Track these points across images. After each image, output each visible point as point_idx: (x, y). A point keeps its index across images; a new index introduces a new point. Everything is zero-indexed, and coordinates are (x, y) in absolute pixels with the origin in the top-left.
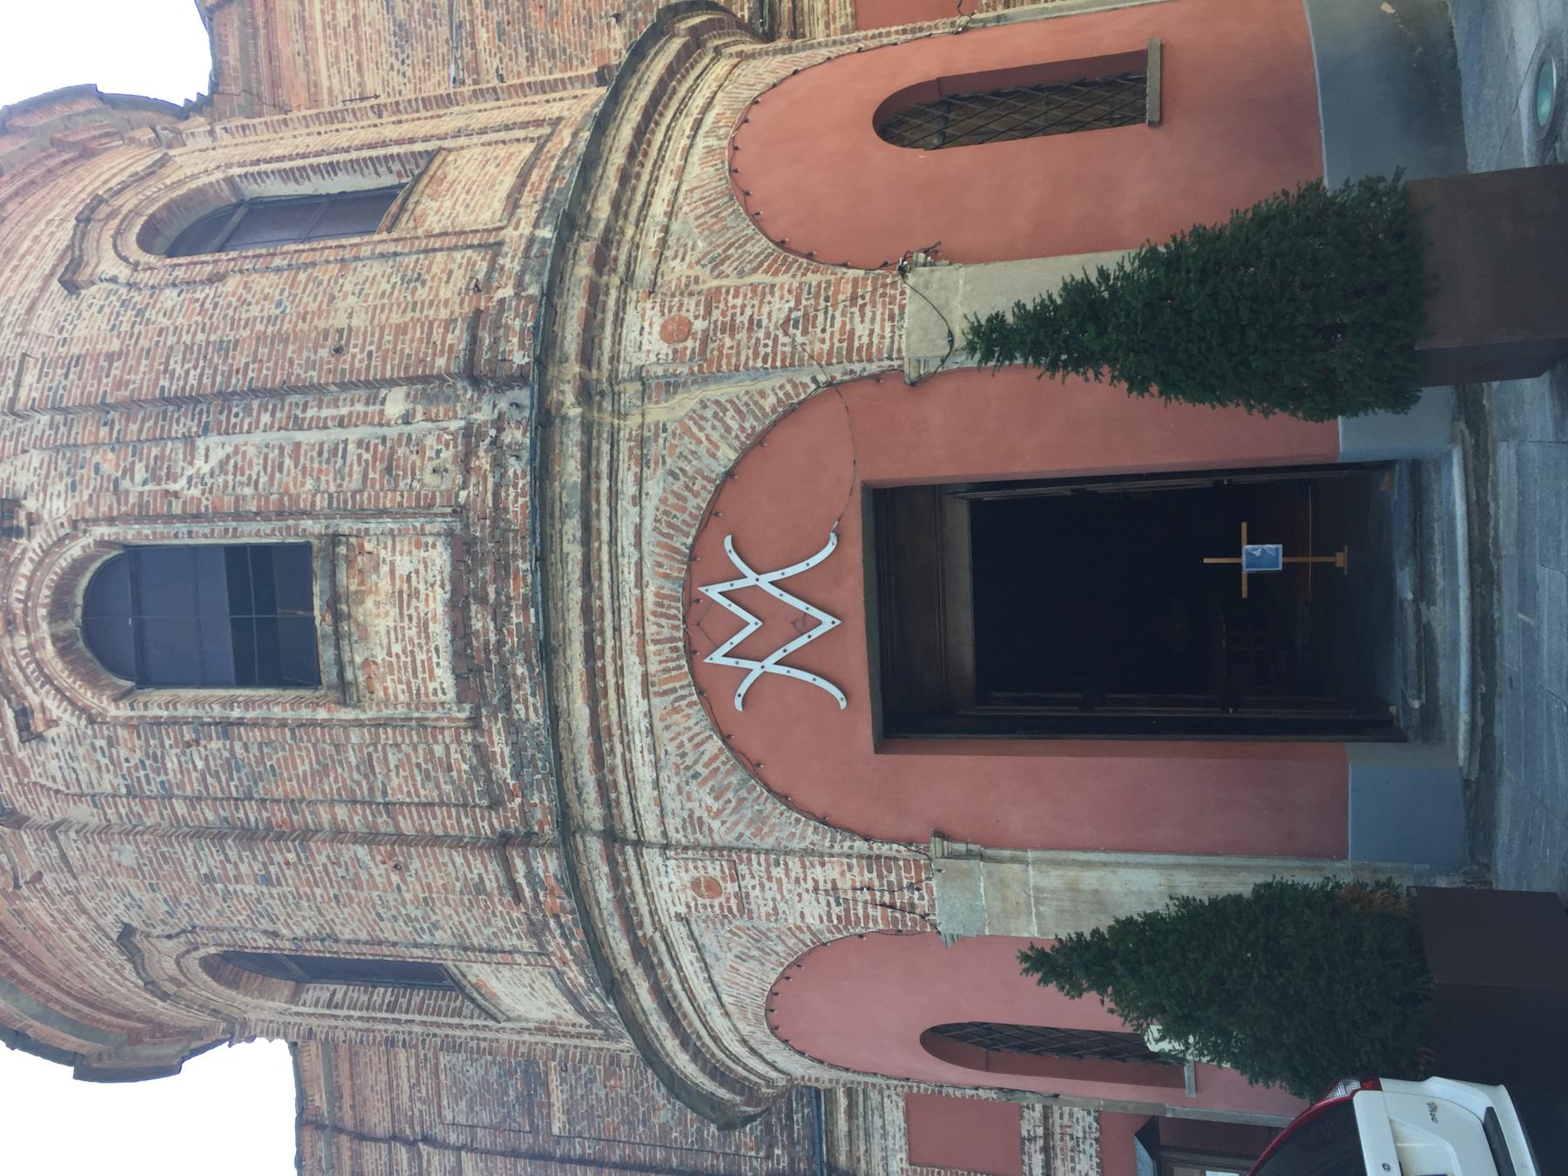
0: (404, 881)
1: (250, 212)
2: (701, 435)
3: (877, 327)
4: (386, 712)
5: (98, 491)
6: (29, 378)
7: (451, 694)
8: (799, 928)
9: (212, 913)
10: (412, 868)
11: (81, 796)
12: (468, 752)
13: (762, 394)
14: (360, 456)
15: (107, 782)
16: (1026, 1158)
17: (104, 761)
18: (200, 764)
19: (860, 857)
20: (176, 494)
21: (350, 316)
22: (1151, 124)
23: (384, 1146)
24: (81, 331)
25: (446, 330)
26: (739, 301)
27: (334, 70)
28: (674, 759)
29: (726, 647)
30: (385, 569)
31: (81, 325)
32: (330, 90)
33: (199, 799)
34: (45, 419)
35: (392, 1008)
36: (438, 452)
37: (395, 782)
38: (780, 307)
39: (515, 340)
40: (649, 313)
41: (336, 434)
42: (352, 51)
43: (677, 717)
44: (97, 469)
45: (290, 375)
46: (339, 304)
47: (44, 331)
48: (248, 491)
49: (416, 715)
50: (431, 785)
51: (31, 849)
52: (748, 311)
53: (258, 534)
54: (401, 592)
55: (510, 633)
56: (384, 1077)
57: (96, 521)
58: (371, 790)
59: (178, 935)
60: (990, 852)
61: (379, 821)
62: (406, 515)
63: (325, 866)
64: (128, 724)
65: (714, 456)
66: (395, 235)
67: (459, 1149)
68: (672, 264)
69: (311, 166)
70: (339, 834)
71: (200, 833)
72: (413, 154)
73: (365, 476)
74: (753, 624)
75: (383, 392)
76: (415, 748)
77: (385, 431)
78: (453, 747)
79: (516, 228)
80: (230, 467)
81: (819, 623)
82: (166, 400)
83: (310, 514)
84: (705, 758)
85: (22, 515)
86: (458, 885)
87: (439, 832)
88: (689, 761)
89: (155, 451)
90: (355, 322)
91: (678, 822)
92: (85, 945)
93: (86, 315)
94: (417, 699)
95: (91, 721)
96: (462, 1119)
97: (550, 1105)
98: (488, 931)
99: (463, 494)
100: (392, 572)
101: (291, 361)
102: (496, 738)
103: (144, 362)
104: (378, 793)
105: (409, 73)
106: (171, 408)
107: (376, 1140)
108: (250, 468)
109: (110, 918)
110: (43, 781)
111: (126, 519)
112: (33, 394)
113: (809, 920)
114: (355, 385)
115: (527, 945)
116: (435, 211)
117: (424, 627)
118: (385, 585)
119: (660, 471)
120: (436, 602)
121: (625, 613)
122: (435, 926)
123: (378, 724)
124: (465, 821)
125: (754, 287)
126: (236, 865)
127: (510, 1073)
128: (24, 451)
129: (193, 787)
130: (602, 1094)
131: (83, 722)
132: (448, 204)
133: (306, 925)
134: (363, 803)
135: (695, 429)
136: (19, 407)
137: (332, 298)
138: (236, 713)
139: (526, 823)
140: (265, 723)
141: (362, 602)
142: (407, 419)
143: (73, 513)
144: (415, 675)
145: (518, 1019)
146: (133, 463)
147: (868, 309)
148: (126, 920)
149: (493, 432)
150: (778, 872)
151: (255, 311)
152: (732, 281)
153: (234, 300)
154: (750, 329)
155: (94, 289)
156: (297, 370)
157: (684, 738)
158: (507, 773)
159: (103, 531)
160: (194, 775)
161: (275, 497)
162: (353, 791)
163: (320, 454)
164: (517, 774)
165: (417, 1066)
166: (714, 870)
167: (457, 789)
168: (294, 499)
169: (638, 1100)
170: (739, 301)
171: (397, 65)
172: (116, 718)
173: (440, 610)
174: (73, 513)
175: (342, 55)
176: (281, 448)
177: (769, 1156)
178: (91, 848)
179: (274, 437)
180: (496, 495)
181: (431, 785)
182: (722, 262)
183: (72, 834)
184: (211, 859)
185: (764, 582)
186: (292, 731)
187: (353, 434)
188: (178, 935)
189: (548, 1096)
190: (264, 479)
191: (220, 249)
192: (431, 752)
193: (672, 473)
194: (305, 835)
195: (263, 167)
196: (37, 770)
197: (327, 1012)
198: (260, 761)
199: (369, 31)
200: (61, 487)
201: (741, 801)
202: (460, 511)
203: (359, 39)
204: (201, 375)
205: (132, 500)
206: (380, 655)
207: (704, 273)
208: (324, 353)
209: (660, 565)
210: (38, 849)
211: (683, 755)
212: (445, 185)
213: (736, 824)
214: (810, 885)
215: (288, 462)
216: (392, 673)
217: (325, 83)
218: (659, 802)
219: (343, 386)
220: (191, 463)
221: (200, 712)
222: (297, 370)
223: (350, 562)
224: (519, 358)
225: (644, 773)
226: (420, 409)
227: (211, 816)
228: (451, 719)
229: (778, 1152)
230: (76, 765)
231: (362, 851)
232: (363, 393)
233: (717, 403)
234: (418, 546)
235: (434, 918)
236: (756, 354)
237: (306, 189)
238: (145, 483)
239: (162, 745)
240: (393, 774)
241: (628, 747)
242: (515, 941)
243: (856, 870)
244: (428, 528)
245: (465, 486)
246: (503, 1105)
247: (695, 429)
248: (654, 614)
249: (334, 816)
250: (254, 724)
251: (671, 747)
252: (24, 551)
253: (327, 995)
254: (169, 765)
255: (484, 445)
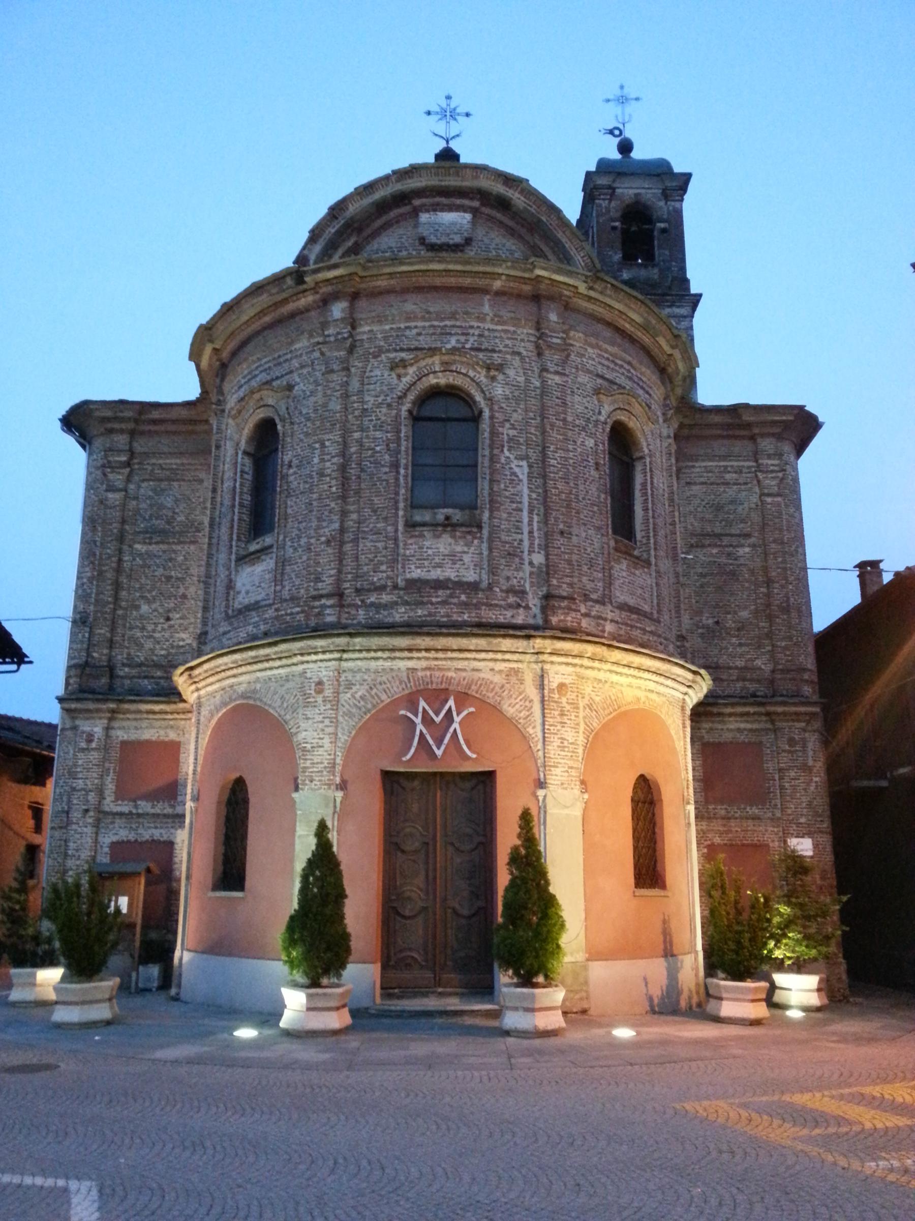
0: (322, 543)
1: (628, 464)
2: (518, 700)
3: (559, 778)
4: (401, 545)
5: (505, 413)
6: (557, 379)
7: (408, 576)
8: (299, 727)
9: (302, 436)
10: (328, 548)
11: (363, 384)
12: (383, 582)
13: (534, 728)
14: (515, 540)
15: (370, 400)
16: (126, 802)
17: (380, 400)
18: (378, 448)
19: (335, 759)
20: (502, 451)
21: (577, 535)
22: (634, 892)
23: (127, 448)
24: (577, 398)
25: (568, 584)
26: (573, 718)
27: (703, 470)
28: (379, 679)
29: (427, 708)
30: (466, 549)
31: (579, 399)
32: (693, 467)
33: (361, 445)
34: (538, 384)
35: (241, 505)
36: (516, 578)
37: (369, 544)
38: (570, 735)
39: (562, 618)
40: (570, 677)
41: (526, 530)
42: (712, 480)
43: (398, 683)
44: (515, 411)
45: (552, 510)
46: (582, 528)
47: (579, 379)
48: (502, 486)
49: (400, 559)
50: (367, 561)
51: (336, 354)
52: (568, 722)
53: (482, 489)
54: (455, 556)
55: (437, 608)
56: (166, 450)
57: (491, 410)
58: (364, 532)
59: (289, 413)
60: (336, 816)
61: (350, 534)
62: (489, 561)
63: (329, 505)
64: (398, 416)
65: (509, 705)
66: (612, 551)
67: (126, 491)
68: (591, 686)
69: (647, 499)
70: (344, 514)
71: (345, 445)
72: (649, 550)
73: (506, 543)
74: (438, 720)
75: (543, 552)
76: (384, 556)
77: (526, 553)
78: (384, 575)
79: (611, 611)
80: (513, 477)
81: (439, 749)
82: (544, 448)
83: (491, 517)
84: (380, 694)
85: (496, 373)
86: (320, 569)
87: (344, 562)
88: (378, 686)
89: (521, 440)
90: (574, 538)
91: (350, 678)
92: (282, 360)
93: (585, 400)
94: (407, 559)
95: (400, 398)
96: (142, 491)
97: (150, 544)
98: (293, 576)
99: (498, 590)
100: (464, 552)
101: (558, 510)
102: (389, 597)
103: (561, 437)
104: (363, 535)
105: (699, 509)
106: (540, 448)
107: (130, 443)
108: (513, 487)
109: (298, 380)
110: (370, 366)
111: (492, 426)
112: (550, 382)
113: (304, 733)
114: (547, 539)
115: (286, 594)
116: (621, 569)
117: (439, 565)
118: (459, 549)
119: (504, 681)
120: (449, 573)
121: (444, 663)
122: (295, 549)
123: (396, 539)
124: (350, 576)
125: (578, 724)
126: (329, 461)
127: (168, 523)
128: (524, 373)
129: (367, 443)
130: (156, 573)
131: (399, 394)
132: (624, 574)
133: (295, 483)
134: (359, 527)
135: (521, 697)
136: (545, 374)
137: (585, 525)
138: (402, 471)
139: (349, 606)
140: (397, 485)
141: (451, 537)
142: (531, 563)
143: (496, 399)
144: (418, 559)
145: (237, 571)
146: (516, 429)
147: (566, 774)
148: (296, 388)
149: (523, 604)
150: (327, 722)
151: (581, 487)
152: (581, 714)
153: (587, 476)
154: (561, 723)
155: (596, 402)
156: (554, 513)
157: (389, 685)
158: (372, 599)
159: (486, 413)
160: (373, 445)
161: (499, 499)
162: (364, 523)
163: (518, 521)
164: (372, 604)
165: (172, 469)
166: (328, 692)
167: (365, 574)
168: (498, 509)
169: (154, 593)
170: (573, 718)
171: (704, 503)
172: (401, 410)
173: (447, 574)
174: (496, 399)
175: (710, 474)
176: (520, 503)
177: (124, 665)
178: (338, 388)
179: (526, 500)
180: (497, 605)
181: (367, 561)
182: (590, 709)
183: (345, 379)
184: (333, 449)
185: (456, 725)
186: (394, 498)
187: (526, 536)
188: (289, 413)
189: (157, 543)
190: (507, 494)
191: (610, 453)
192: (382, 564)
193: (503, 686)
194: (344, 498)
195: (649, 474)
196: (376, 364)
197: (239, 470)
198: (380, 479)
199: (722, 490)
200: (507, 393)
201: (360, 709)
202: (490, 587)
203: (718, 484)
204: (554, 466)
205: (500, 429)
206: (427, 544)
207: (586, 701)
208: (561, 526)
209: (464, 679)
210: (337, 358)
211: (381, 684)
212: (633, 570)
213: (349, 705)
214: (322, 736)
215: (514, 505)
216: (419, 548)
217: (697, 464)
218: (359, 670)
219: (546, 534)
220: (516, 458)
221: (403, 453)
222: (554, 513)
223: (469, 533)
224: (554, 620)
225: (373, 664)
226: (535, 570)
227: (353, 450)
228: (397, 576)
229: (126, 669)
230: (378, 384)
231: (337, 526)
232: (543, 543)
233: (532, 707)
234: (475, 565)
235: (300, 550)
236: (551, 725)
237: (638, 494)
238: (508, 435)
239: (387, 432)
240: (372, 544)
241: (385, 659)
242: (287, 588)
243: (328, 757)
244: (483, 571)
245: (502, 591)
246: (151, 516)
247: (521, 697)
248: (443, 676)
249: (352, 512)
250: (397, 479)
251: (384, 679)
252: (479, 373)
253: (247, 469)
254: (378, 433)
255: (518, 600)
